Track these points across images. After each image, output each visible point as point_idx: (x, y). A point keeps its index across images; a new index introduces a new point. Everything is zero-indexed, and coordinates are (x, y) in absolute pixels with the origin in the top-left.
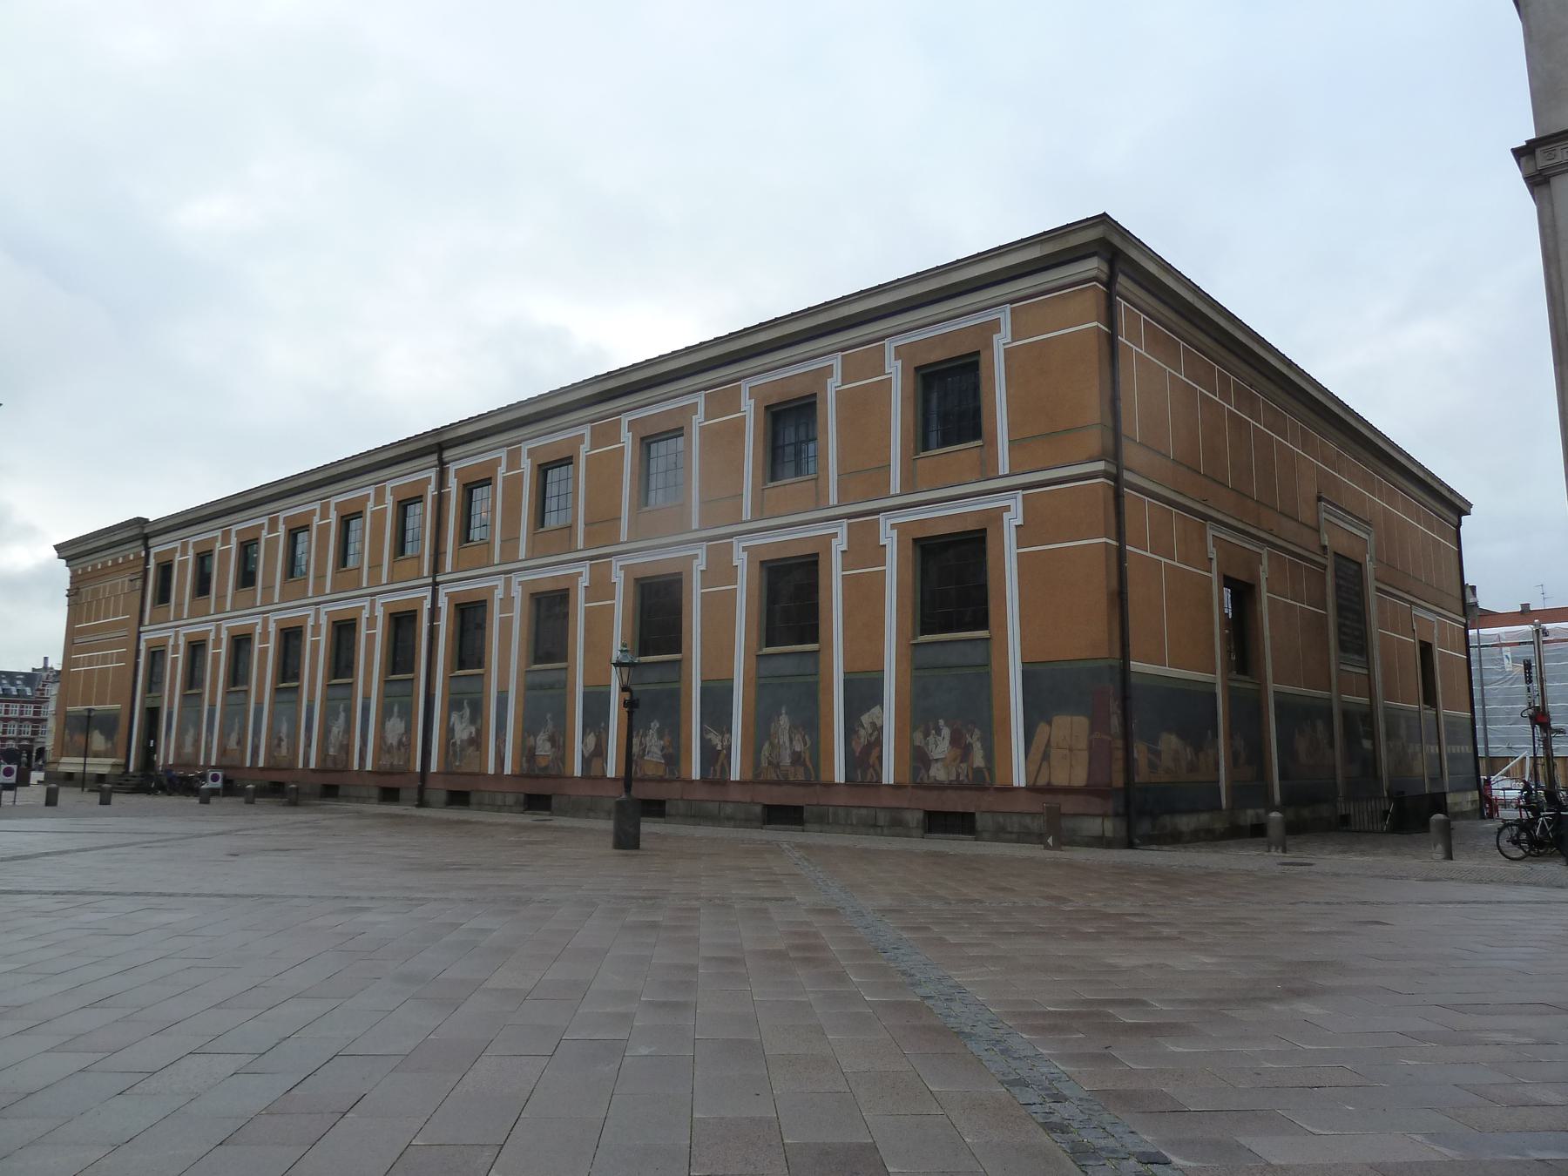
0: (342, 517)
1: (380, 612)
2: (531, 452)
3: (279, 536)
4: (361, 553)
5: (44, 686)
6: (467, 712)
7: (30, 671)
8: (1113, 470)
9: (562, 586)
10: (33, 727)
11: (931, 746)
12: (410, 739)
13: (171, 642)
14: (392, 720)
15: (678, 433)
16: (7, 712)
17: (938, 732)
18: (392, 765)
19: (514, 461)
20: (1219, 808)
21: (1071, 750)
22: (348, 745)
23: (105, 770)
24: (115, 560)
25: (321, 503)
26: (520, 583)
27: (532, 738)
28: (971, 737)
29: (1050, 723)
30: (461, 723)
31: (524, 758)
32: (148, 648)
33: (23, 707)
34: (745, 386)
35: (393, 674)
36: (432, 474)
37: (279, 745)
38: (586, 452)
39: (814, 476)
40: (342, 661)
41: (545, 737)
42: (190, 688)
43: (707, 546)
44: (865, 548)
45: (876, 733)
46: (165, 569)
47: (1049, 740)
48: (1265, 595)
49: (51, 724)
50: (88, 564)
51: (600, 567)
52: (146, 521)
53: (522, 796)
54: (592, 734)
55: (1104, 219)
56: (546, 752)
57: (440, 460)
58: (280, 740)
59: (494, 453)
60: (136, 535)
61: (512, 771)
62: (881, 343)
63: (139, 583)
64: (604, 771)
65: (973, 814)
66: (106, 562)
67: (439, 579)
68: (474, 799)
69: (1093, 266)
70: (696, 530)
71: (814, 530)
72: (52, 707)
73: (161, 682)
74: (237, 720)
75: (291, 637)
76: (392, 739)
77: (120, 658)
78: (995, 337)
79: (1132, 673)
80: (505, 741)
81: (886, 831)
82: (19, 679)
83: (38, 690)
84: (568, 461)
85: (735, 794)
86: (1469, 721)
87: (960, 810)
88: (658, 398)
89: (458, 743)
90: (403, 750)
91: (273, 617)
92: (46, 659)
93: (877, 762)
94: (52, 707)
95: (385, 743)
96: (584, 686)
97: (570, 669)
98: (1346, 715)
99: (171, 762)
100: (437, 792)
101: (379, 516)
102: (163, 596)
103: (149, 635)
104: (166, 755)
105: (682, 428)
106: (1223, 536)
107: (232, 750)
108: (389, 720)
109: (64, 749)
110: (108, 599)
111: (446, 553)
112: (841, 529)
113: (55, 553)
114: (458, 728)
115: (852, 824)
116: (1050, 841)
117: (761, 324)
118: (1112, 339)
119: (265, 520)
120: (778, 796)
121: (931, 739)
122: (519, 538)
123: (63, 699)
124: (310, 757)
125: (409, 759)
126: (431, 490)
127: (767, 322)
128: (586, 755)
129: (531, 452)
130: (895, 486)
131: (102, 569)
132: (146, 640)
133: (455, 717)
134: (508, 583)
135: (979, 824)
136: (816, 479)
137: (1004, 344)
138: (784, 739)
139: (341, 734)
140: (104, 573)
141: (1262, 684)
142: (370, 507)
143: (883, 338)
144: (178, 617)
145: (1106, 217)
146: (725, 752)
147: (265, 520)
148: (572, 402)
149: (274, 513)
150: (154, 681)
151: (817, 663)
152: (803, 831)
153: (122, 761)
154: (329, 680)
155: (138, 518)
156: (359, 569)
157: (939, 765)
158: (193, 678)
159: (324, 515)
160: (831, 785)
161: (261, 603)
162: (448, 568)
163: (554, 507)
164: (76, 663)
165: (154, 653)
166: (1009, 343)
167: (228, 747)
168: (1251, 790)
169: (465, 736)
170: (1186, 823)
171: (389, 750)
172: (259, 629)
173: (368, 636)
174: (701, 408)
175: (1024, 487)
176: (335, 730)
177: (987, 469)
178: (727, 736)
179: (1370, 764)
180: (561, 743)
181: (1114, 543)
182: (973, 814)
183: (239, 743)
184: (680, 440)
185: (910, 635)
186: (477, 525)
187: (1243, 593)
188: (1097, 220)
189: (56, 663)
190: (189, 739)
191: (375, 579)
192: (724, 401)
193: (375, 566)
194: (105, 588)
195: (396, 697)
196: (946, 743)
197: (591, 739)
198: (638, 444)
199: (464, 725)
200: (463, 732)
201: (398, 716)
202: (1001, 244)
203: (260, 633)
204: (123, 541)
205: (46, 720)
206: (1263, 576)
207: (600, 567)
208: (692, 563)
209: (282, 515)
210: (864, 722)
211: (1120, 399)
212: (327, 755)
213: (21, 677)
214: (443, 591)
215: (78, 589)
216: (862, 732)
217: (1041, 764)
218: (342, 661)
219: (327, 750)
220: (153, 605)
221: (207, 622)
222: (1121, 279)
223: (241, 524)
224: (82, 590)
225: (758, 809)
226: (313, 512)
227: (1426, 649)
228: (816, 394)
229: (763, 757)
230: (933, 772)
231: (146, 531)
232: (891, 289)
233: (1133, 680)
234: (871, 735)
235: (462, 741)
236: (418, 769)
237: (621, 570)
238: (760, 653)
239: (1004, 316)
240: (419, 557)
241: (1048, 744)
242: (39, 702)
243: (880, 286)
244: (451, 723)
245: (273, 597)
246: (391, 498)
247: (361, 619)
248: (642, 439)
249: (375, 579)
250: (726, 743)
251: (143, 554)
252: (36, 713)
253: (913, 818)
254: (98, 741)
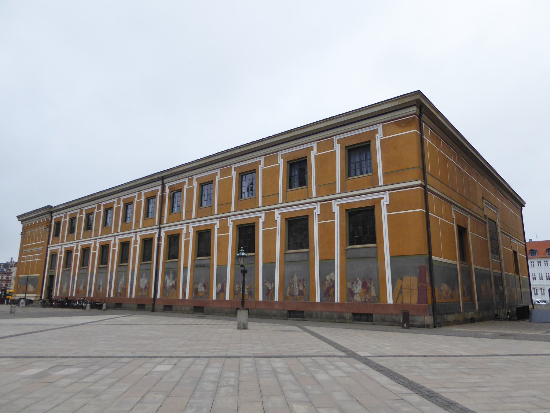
0: (105, 209)
1: (117, 242)
2: (197, 179)
3: (83, 216)
4: (132, 217)
5: (11, 268)
6: (172, 275)
7: (6, 263)
8: (424, 184)
9: (209, 228)
10: (6, 283)
11: (354, 288)
12: (149, 286)
13: (59, 251)
14: (143, 278)
15: (154, 197)
16: (2, 278)
17: (357, 283)
18: (142, 296)
19: (139, 197)
20: (461, 312)
21: (410, 289)
22: (125, 289)
23: (33, 299)
24: (39, 222)
25: (188, 179)
26: (193, 227)
27: (196, 285)
28: (370, 284)
29: (402, 279)
30: (169, 279)
31: (193, 293)
32: (51, 253)
33: (3, 276)
34: (279, 154)
35: (121, 263)
36: (160, 188)
37: (99, 289)
38: (218, 179)
39: (254, 197)
40: (124, 257)
41: (202, 285)
42: (66, 268)
43: (265, 213)
44: (270, 220)
45: (332, 283)
46: (58, 224)
47: (402, 286)
48: (470, 233)
49: (13, 281)
50: (29, 223)
51: (270, 215)
52: (52, 207)
53: (193, 307)
54: (220, 283)
55: (419, 92)
56: (202, 290)
57: (163, 182)
58: (100, 286)
59: (112, 200)
60: (47, 212)
61: (189, 298)
62: (277, 153)
63: (48, 230)
64: (225, 298)
65: (372, 314)
66: (32, 223)
67: (161, 226)
68: (174, 308)
69: (414, 110)
70: (141, 228)
71: (363, 198)
72: (14, 275)
73: (55, 265)
74: (83, 279)
75: (105, 248)
76: (142, 286)
77: (40, 257)
78: (376, 135)
79: (433, 261)
80: (186, 286)
81: (337, 321)
82: (1, 266)
83: (9, 269)
84: (211, 182)
85: (276, 307)
86: (518, 278)
87: (366, 312)
88: (371, 124)
89: (168, 287)
90: (146, 290)
91: (98, 241)
92: (12, 258)
93: (333, 294)
94: (14, 275)
95: (140, 288)
96: (217, 266)
97: (256, 257)
98: (495, 277)
99: (58, 295)
100: (159, 306)
101: (139, 203)
102: (57, 234)
103: (52, 248)
104: (56, 292)
105: (255, 169)
106: (456, 210)
107: (81, 290)
108: (141, 279)
109: (17, 291)
110: (29, 237)
111: (164, 216)
112: (263, 215)
113: (17, 219)
114: (168, 281)
115: (323, 318)
116: (405, 325)
117: (286, 131)
118: (421, 136)
119: (96, 206)
120: (293, 307)
121: (354, 285)
122: (192, 211)
123: (18, 273)
124: (132, 293)
125: (149, 293)
126: (159, 194)
127: (282, 133)
128: (218, 291)
129: (197, 179)
130: (338, 190)
131: (34, 224)
132: (50, 250)
133: (167, 277)
134: (115, 239)
135: (374, 318)
136: (307, 188)
137: (380, 138)
138: (296, 285)
139: (123, 284)
140: (36, 226)
141: (470, 265)
142: (115, 206)
143: (333, 136)
144: (62, 242)
145: (420, 92)
146: (272, 290)
147: (96, 206)
148: (378, 111)
149: (99, 203)
150: (52, 266)
151: (308, 256)
152: (304, 320)
153: (40, 295)
154: (119, 264)
155: (48, 206)
156: (131, 223)
157: (358, 295)
158: (67, 264)
159: (119, 203)
160: (315, 304)
161: (94, 236)
162: (165, 222)
163: (206, 199)
164: (24, 259)
165: (52, 255)
166: (263, 167)
167: (80, 290)
168: (469, 305)
169: (171, 284)
170: (451, 318)
171: (141, 290)
172: (93, 246)
173: (134, 247)
174: (219, 174)
175: (389, 190)
176: (121, 283)
177: (308, 195)
178: (273, 284)
179: (501, 295)
180: (208, 287)
181: (424, 211)
182: (372, 314)
183: (84, 288)
184: (92, 215)
185: (345, 246)
186: (176, 206)
187: (462, 231)
188: (417, 92)
189: (16, 260)
190: (65, 287)
191: (137, 226)
192: (226, 172)
193: (137, 221)
194: (35, 231)
195: (144, 271)
196: (360, 286)
197: (220, 286)
198: (238, 176)
199: (170, 280)
200: (170, 283)
201: (145, 277)
202: (405, 94)
203: (113, 244)
204: (45, 213)
205: (11, 280)
206: (469, 225)
207: (270, 215)
208: (390, 202)
209: (103, 204)
210: (327, 278)
211: (425, 158)
212: (117, 292)
213: (3, 265)
214: (163, 231)
215: (25, 232)
216: (327, 283)
217: (399, 295)
218: (124, 257)
219: (117, 290)
220: (53, 237)
221: (73, 243)
222: (423, 115)
223: (87, 207)
224: (27, 232)
225: (286, 312)
226: (114, 202)
227: (515, 253)
228: (307, 156)
229: (287, 292)
230: (355, 298)
231: (51, 210)
232: (336, 118)
233: (434, 263)
234: (330, 284)
235: (169, 286)
236: (152, 297)
237: (231, 222)
238: (286, 252)
239: (380, 128)
240: (154, 218)
241: (401, 287)
242: (9, 274)
243: (332, 117)
244: (165, 280)
245: (98, 234)
246: (144, 197)
247: (91, 247)
248: (240, 174)
249: (137, 226)
250: (272, 287)
251: (50, 219)
252: (8, 278)
253: (348, 315)
254: (30, 288)
